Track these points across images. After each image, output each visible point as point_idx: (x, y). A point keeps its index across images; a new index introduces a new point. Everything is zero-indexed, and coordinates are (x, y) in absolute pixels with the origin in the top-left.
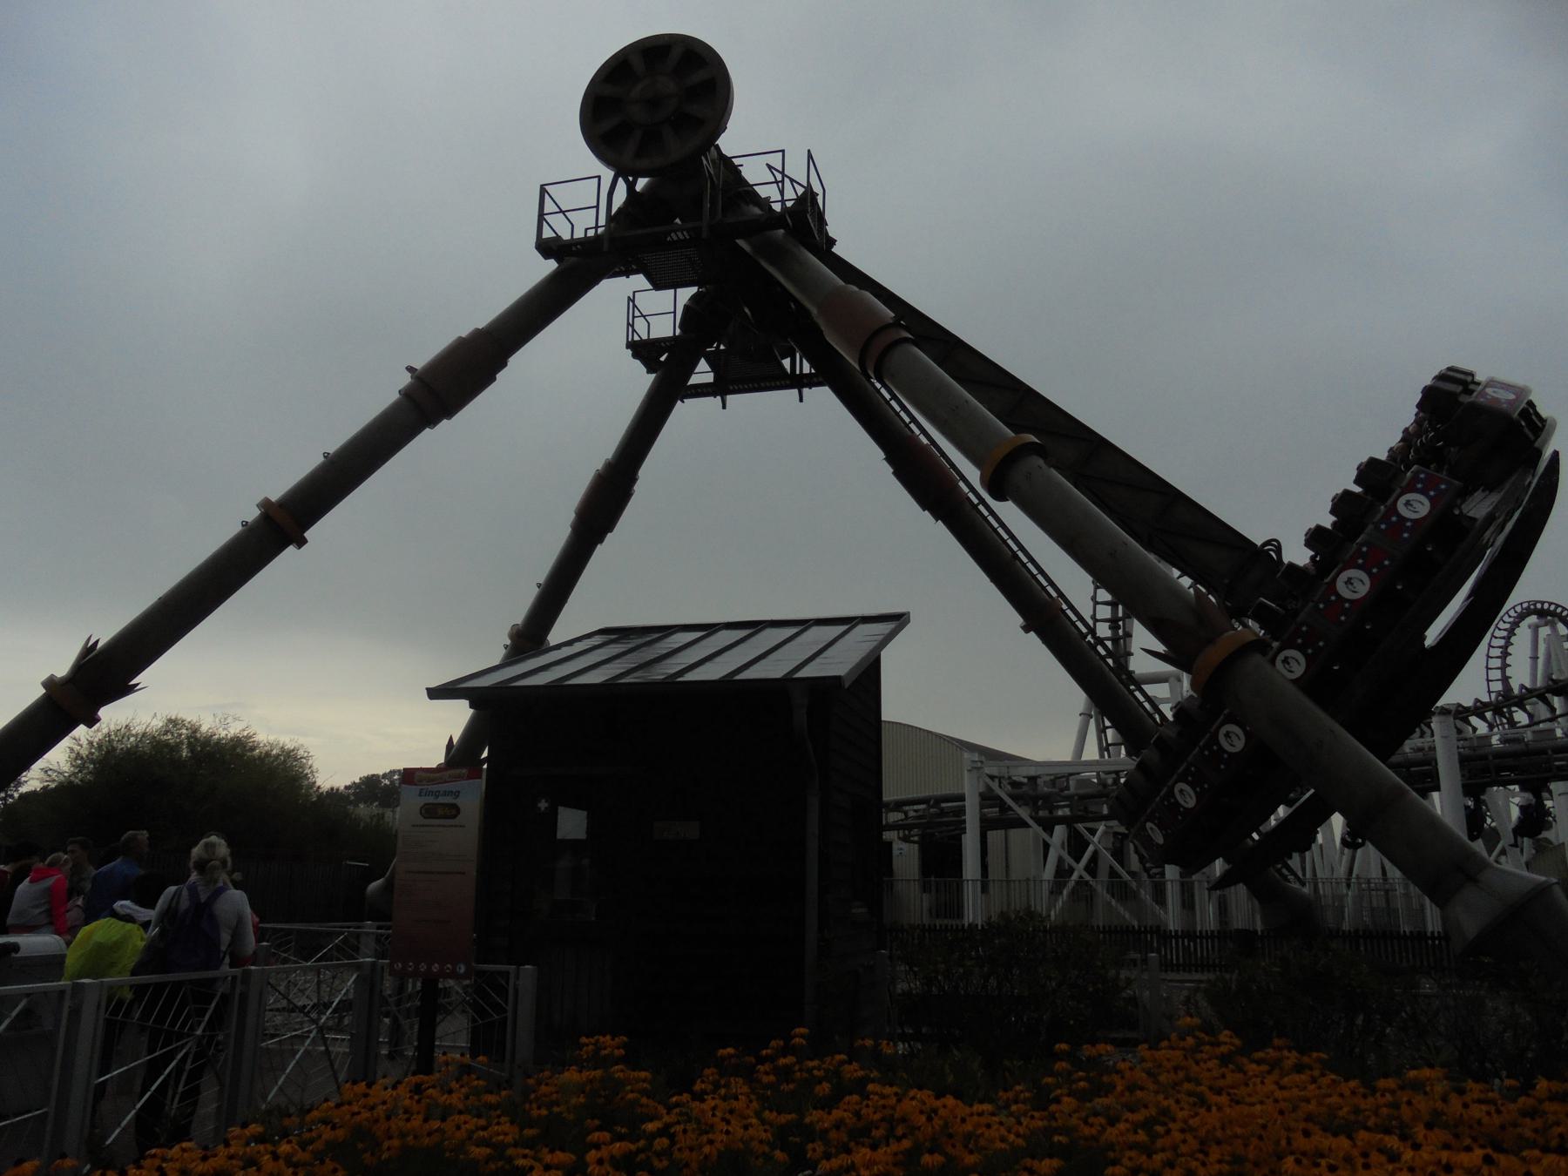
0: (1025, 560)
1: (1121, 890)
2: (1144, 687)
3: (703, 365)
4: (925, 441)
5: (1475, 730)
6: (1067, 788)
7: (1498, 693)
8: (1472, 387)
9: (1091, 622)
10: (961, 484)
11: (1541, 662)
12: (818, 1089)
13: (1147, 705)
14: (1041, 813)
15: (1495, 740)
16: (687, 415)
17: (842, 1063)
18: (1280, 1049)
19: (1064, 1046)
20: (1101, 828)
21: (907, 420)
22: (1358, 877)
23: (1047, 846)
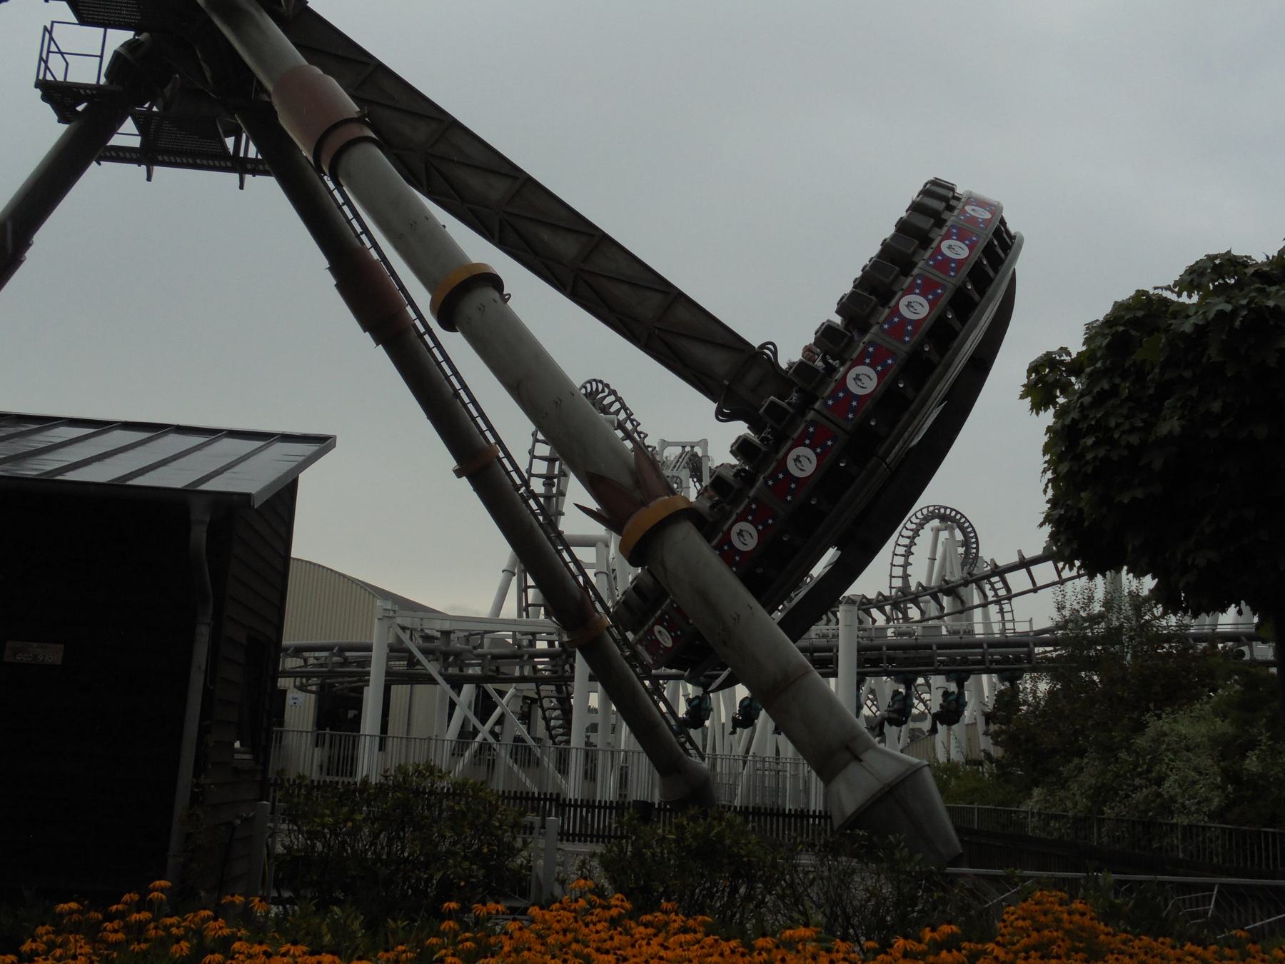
0: (466, 400)
1: (522, 753)
2: (576, 550)
3: (129, 125)
4: (375, 256)
5: (874, 621)
6: (481, 646)
7: (899, 589)
8: (953, 202)
9: (526, 476)
10: (409, 309)
11: (937, 563)
12: (175, 948)
13: (571, 565)
14: (450, 670)
15: (890, 632)
16: (99, 178)
17: (205, 920)
18: (666, 912)
19: (453, 905)
20: (511, 691)
21: (359, 230)
22: (754, 755)
23: (453, 705)
